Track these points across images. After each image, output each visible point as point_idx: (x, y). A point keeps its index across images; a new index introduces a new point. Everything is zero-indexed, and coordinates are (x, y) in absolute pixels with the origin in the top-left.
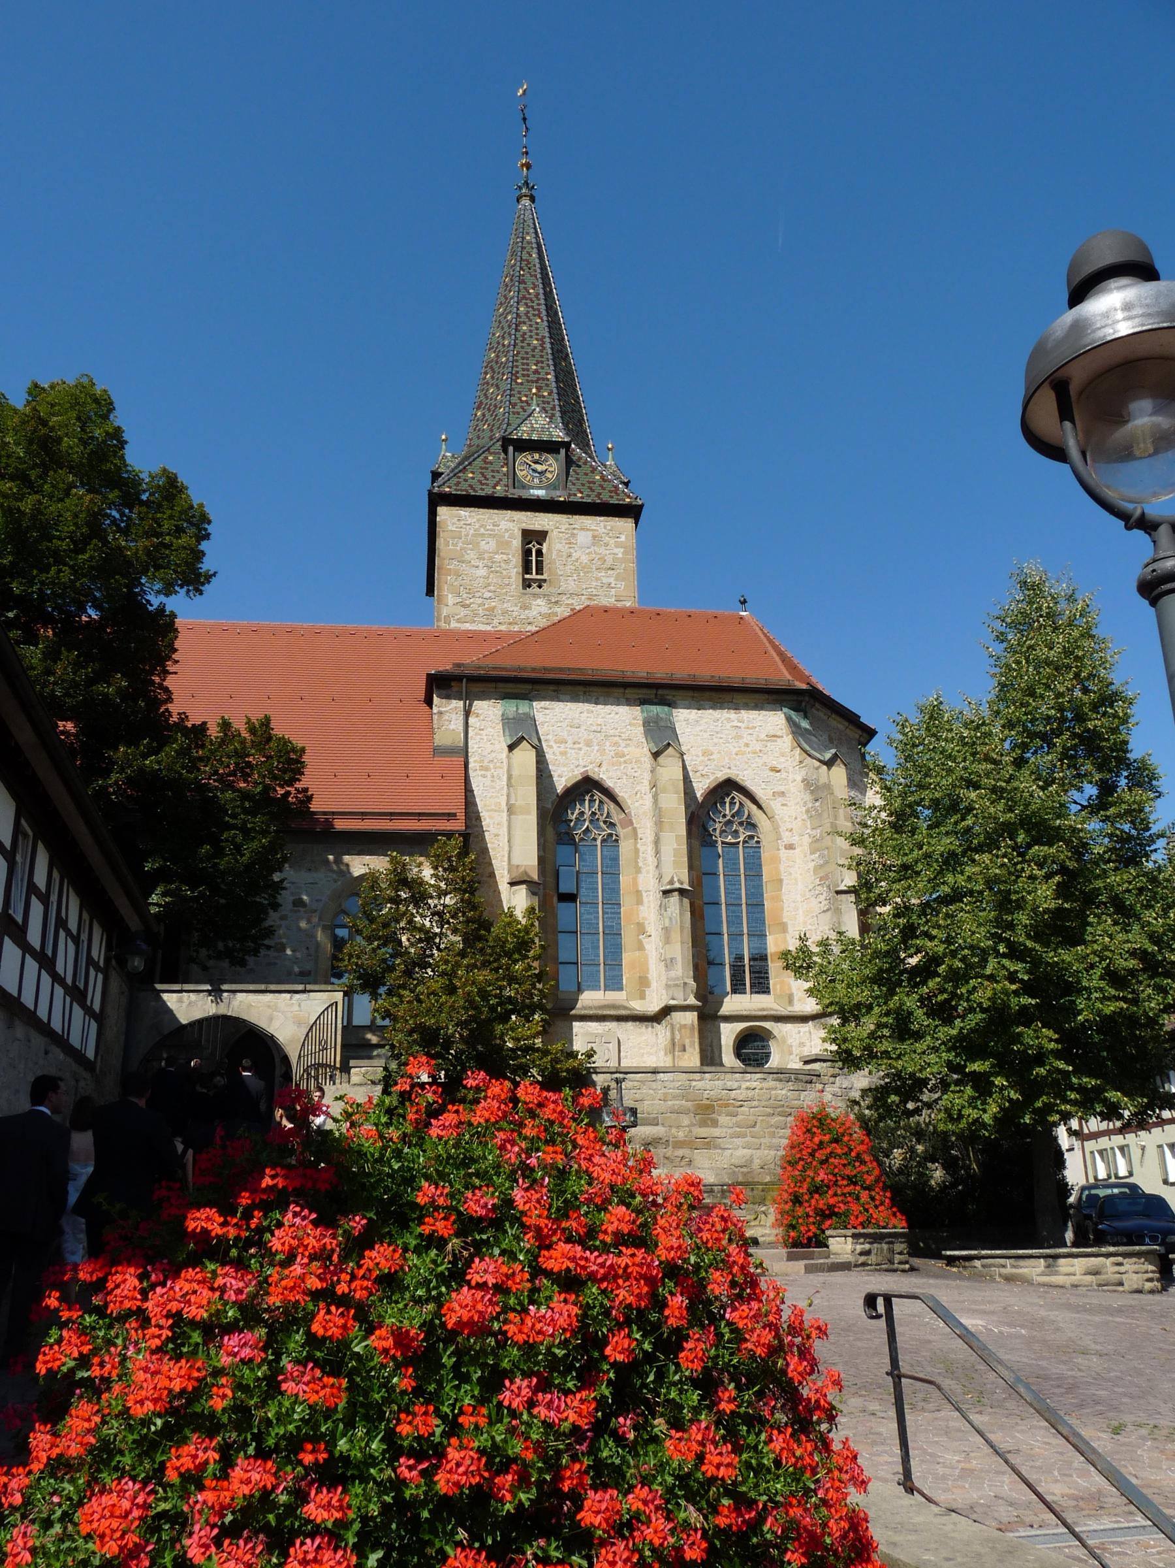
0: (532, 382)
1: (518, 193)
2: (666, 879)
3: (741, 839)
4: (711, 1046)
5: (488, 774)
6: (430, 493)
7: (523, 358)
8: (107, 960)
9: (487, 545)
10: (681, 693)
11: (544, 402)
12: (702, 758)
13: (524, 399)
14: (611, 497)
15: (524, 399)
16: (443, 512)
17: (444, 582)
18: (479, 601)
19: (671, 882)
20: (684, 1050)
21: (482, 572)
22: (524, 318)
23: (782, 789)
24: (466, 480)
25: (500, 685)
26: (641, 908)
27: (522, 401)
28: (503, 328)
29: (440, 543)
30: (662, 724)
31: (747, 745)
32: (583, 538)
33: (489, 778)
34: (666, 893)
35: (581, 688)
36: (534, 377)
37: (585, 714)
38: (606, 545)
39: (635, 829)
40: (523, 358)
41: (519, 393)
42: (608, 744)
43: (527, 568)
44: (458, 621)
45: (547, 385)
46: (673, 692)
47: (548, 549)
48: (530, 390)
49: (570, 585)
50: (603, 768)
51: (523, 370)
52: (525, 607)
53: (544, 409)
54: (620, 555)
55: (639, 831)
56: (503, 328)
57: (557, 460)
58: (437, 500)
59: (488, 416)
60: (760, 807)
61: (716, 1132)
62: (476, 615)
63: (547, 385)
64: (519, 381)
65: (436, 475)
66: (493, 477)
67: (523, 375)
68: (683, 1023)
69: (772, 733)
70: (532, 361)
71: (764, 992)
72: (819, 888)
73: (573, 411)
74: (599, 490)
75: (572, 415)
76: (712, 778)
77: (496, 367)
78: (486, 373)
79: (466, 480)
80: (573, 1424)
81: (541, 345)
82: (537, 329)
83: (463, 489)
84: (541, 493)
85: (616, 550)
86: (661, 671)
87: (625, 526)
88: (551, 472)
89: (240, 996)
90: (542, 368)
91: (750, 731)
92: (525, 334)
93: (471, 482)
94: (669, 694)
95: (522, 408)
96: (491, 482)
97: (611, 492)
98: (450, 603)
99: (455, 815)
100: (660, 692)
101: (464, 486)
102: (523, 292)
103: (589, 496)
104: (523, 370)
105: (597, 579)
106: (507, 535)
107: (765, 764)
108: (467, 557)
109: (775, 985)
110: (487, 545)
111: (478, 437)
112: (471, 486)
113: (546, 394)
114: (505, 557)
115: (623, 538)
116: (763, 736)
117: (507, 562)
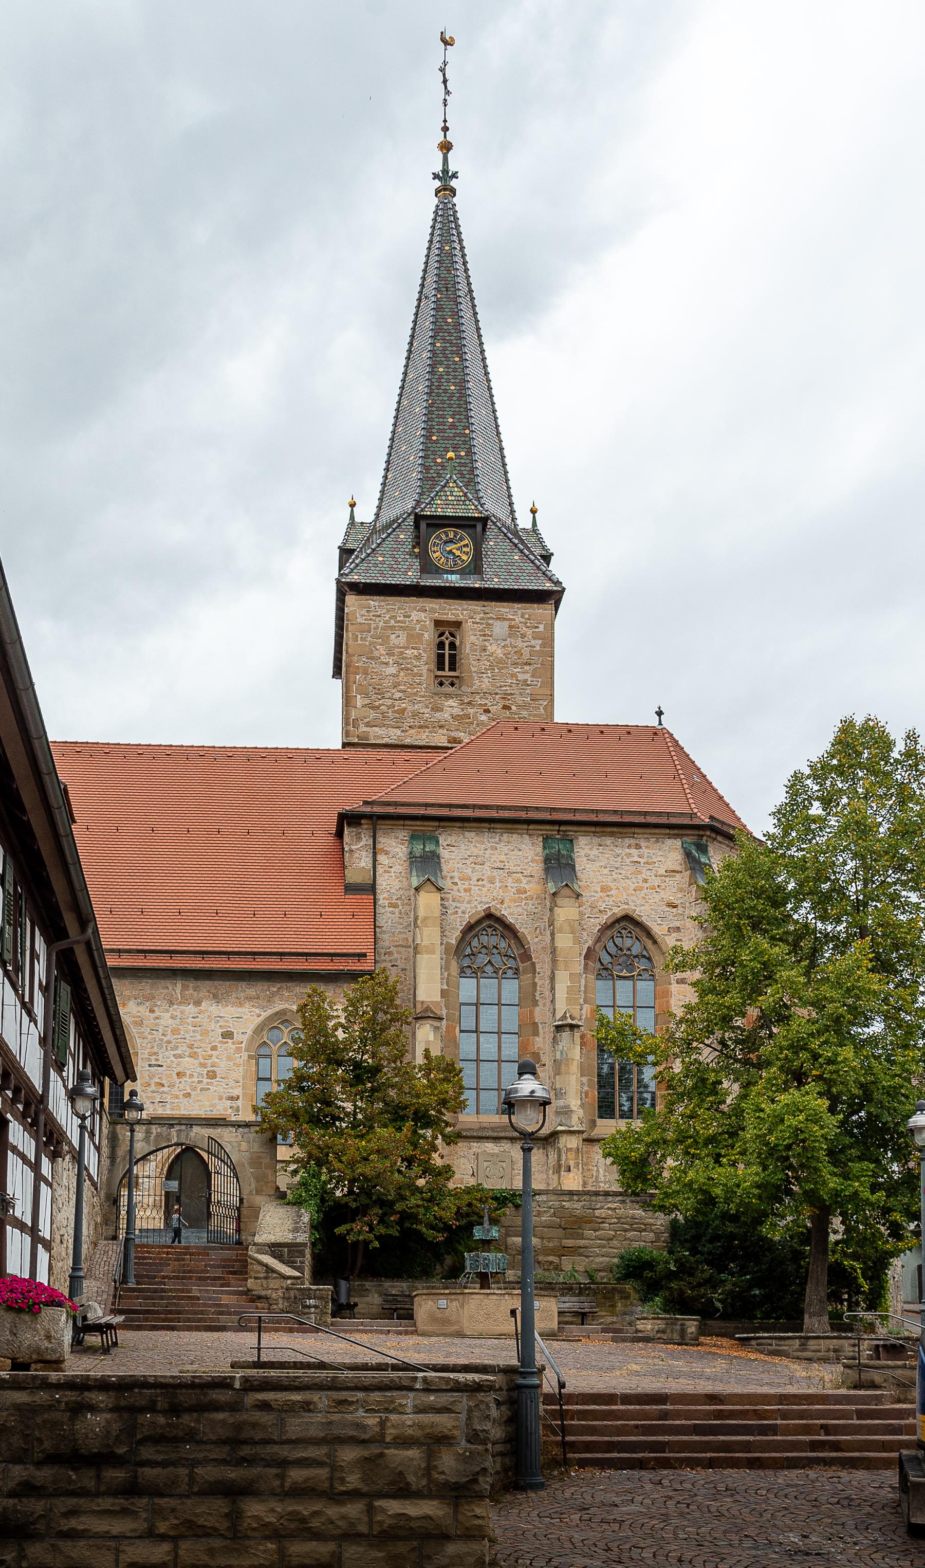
0: (448, 439)
2: (559, 1015)
6: (338, 582)
7: (438, 409)
9: (398, 639)
13: (439, 460)
15: (439, 460)
18: (389, 702)
19: (564, 1017)
20: (569, 1171)
21: (392, 670)
23: (678, 924)
26: (537, 1039)
31: (645, 881)
32: (500, 629)
33: (397, 915)
34: (559, 1028)
36: (450, 433)
37: (489, 851)
42: (510, 880)
43: (440, 666)
44: (368, 725)
47: (461, 642)
50: (505, 905)
52: (437, 709)
54: (538, 648)
55: (537, 966)
60: (655, 942)
61: (582, 1242)
64: (434, 438)
69: (671, 868)
76: (609, 914)
84: (454, 580)
85: (533, 642)
90: (460, 421)
91: (650, 867)
98: (359, 704)
99: (365, 955)
100: (562, 828)
105: (513, 675)
108: (376, 654)
110: (398, 639)
113: (463, 454)
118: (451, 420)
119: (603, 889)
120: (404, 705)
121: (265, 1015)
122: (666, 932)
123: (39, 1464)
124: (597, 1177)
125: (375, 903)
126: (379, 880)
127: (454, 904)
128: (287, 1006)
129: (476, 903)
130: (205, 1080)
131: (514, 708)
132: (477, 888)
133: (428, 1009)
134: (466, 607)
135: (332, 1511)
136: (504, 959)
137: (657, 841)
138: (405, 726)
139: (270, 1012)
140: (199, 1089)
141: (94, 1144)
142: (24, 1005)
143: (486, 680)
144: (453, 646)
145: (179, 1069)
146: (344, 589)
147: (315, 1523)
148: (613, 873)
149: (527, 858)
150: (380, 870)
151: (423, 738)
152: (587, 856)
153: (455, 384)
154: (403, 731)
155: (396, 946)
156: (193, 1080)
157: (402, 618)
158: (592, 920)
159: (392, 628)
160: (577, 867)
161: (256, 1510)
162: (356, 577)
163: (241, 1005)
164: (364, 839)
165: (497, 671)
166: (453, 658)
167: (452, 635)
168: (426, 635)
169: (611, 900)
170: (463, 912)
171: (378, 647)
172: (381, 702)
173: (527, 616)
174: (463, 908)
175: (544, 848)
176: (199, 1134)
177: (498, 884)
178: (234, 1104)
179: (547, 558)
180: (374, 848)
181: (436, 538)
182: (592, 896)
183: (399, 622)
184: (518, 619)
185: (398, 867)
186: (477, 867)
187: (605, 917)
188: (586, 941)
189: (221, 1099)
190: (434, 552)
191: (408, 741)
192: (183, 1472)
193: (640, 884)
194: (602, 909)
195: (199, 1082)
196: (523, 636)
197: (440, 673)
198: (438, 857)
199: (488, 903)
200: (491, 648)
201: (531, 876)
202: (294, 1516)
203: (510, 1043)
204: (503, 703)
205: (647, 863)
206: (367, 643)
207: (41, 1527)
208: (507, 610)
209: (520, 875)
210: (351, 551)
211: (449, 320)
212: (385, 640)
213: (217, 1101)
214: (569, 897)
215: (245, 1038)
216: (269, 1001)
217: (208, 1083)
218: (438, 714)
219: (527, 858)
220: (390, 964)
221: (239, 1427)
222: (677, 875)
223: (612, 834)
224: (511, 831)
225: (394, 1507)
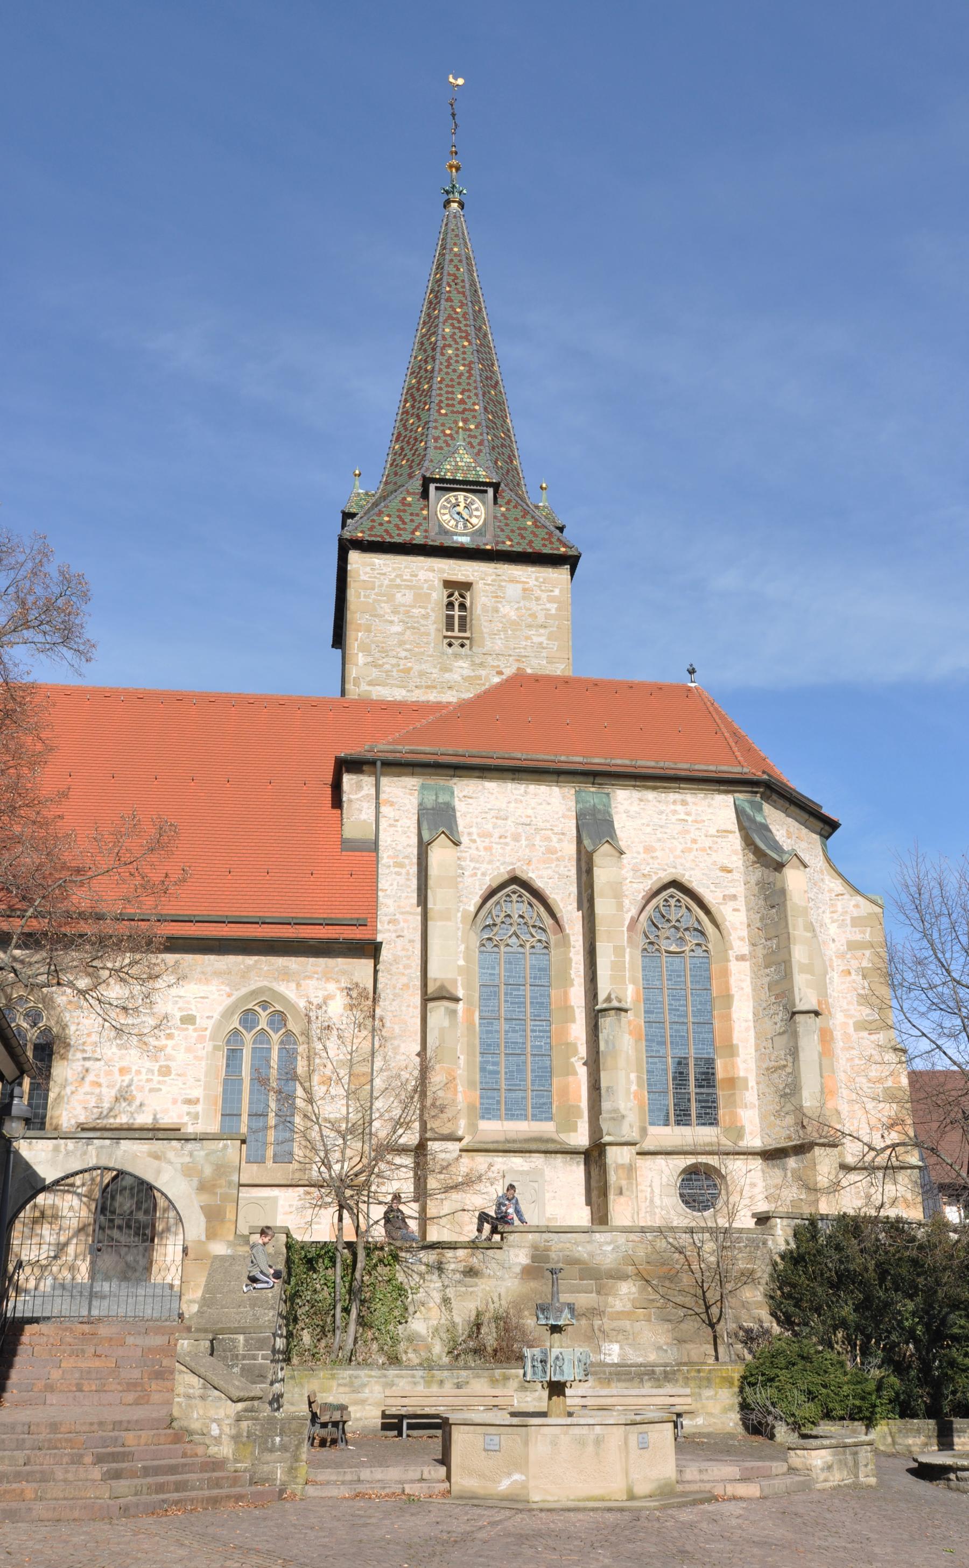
0: (458, 412)
1: (445, 197)
3: (687, 948)
4: (650, 1186)
5: (404, 871)
6: (341, 540)
7: (447, 386)
9: (404, 598)
11: (470, 436)
12: (643, 856)
13: (448, 432)
14: (544, 545)
15: (448, 432)
16: (354, 557)
17: (355, 638)
18: (394, 661)
19: (608, 999)
20: (621, 1193)
21: (397, 628)
22: (450, 341)
24: (381, 524)
27: (446, 435)
28: (425, 351)
30: (600, 817)
31: (694, 841)
32: (513, 591)
36: (459, 408)
37: (513, 805)
38: (538, 599)
40: (447, 386)
41: (443, 425)
42: (538, 838)
43: (450, 626)
44: (370, 683)
45: (474, 417)
47: (472, 603)
48: (456, 422)
49: (498, 644)
51: (447, 399)
52: (445, 669)
53: (470, 443)
54: (553, 611)
56: (425, 351)
57: (484, 503)
59: (407, 451)
60: (707, 912)
63: (474, 417)
64: (443, 411)
65: (347, 516)
66: (412, 521)
67: (448, 405)
68: (620, 1161)
69: (723, 827)
70: (458, 389)
71: (711, 1124)
72: (774, 1007)
73: (503, 446)
74: (531, 537)
75: (502, 448)
76: (655, 878)
77: (417, 395)
78: (406, 401)
79: (381, 524)
80: (575, 1130)
81: (469, 372)
82: (464, 353)
83: (377, 535)
84: (465, 540)
85: (548, 606)
86: (598, 761)
87: (560, 575)
90: (469, 397)
91: (699, 826)
92: (450, 358)
93: (387, 526)
95: (446, 442)
97: (543, 539)
101: (379, 531)
102: (450, 311)
103: (518, 543)
104: (447, 399)
105: (528, 638)
106: (426, 586)
107: (715, 863)
108: (381, 612)
109: (724, 1115)
110: (404, 598)
111: (396, 474)
112: (386, 531)
113: (472, 427)
114: (423, 611)
115: (557, 592)
117: (425, 617)
118: (460, 396)
120: (409, 665)
121: (237, 995)
122: (721, 901)
124: (652, 1201)
127: (472, 865)
128: (266, 983)
129: (498, 864)
130: (156, 1078)
132: (499, 846)
133: (442, 987)
134: (477, 568)
136: (533, 930)
138: (411, 685)
139: (244, 991)
140: (147, 1089)
143: (499, 642)
144: (462, 606)
145: (124, 1064)
146: (345, 547)
148: (658, 832)
149: (557, 813)
150: (383, 824)
152: (626, 812)
153: (464, 365)
154: (408, 691)
155: (402, 913)
156: (140, 1077)
157: (408, 577)
158: (635, 885)
159: (398, 586)
162: (360, 535)
163: (207, 982)
164: (366, 788)
165: (510, 632)
166: (463, 619)
167: (462, 596)
169: (656, 862)
170: (484, 874)
171: (383, 605)
172: (384, 660)
173: (541, 580)
174: (483, 870)
175: (577, 802)
176: (134, 1157)
177: (524, 842)
178: (193, 1109)
180: (377, 797)
181: (446, 500)
182: (633, 858)
183: (405, 580)
184: (532, 582)
185: (405, 820)
186: (500, 822)
187: (650, 882)
188: (629, 910)
189: (175, 1102)
190: (444, 514)
193: (689, 845)
194: (646, 872)
195: (148, 1080)
197: (449, 634)
198: (454, 809)
199: (512, 864)
201: (563, 834)
203: (540, 1031)
205: (696, 821)
206: (371, 601)
208: (520, 573)
209: (550, 832)
211: (458, 310)
212: (391, 598)
214: (611, 856)
215: (210, 1024)
216: (243, 977)
217: (159, 1082)
218: (447, 675)
219: (557, 813)
220: (394, 935)
222: (731, 835)
224: (538, 781)
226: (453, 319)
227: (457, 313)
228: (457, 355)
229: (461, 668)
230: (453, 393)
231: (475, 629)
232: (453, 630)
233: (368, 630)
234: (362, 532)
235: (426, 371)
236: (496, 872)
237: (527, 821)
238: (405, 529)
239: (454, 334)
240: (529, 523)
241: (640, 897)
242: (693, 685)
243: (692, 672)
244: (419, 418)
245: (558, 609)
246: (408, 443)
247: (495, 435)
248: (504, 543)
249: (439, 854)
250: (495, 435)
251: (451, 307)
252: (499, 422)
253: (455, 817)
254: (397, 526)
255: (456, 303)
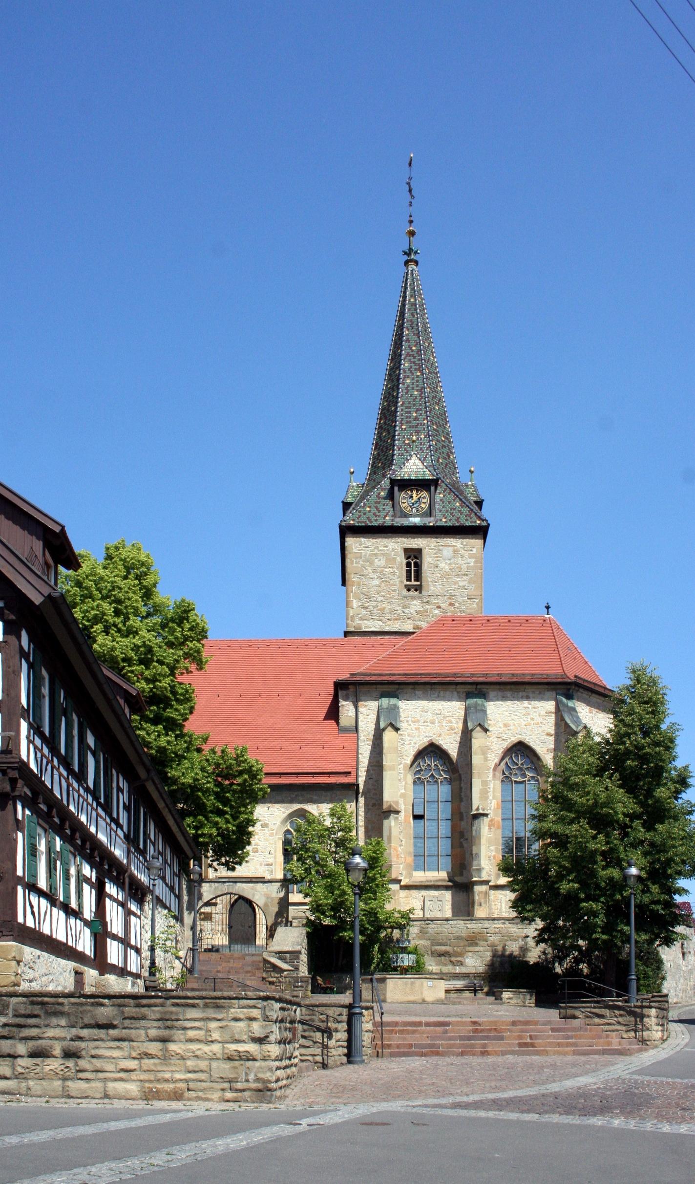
0: (413, 427)
1: (406, 258)
6: (341, 527)
8: (179, 871)
10: (492, 687)
14: (467, 520)
15: (407, 442)
16: (350, 541)
18: (374, 604)
19: (478, 809)
21: (377, 582)
25: (379, 686)
29: (348, 561)
30: (479, 708)
31: (532, 719)
35: (428, 686)
36: (414, 423)
39: (460, 775)
44: (361, 619)
46: (487, 687)
51: (407, 417)
54: (472, 564)
58: (346, 531)
62: (372, 614)
65: (346, 506)
67: (407, 422)
73: (443, 446)
74: (457, 515)
76: (509, 741)
79: (365, 514)
84: (416, 521)
85: (469, 560)
87: (475, 543)
88: (424, 498)
89: (238, 884)
94: (484, 688)
96: (382, 514)
98: (355, 606)
99: (350, 773)
100: (479, 687)
101: (364, 518)
105: (455, 583)
108: (365, 572)
110: (380, 562)
112: (368, 518)
113: (422, 436)
115: (474, 551)
116: (543, 713)
117: (394, 573)
118: (414, 415)
119: (505, 725)
123: (82, 1028)
125: (358, 739)
126: (360, 724)
131: (457, 604)
135: (206, 1048)
137: (540, 693)
141: (175, 894)
142: (112, 820)
146: (346, 531)
147: (198, 1053)
150: (361, 717)
151: (396, 627)
153: (417, 391)
159: (376, 555)
160: (488, 712)
161: (172, 1047)
162: (352, 522)
168: (398, 558)
178: (269, 868)
179: (479, 504)
189: (261, 865)
191: (387, 629)
192: (142, 1032)
196: (462, 557)
197: (408, 583)
200: (442, 565)
202: (188, 1050)
204: (449, 601)
207: (83, 1053)
210: (351, 504)
212: (371, 564)
213: (258, 867)
221: (165, 1013)
223: (511, 690)
225: (233, 1047)
226: (410, 355)
227: (413, 351)
228: (413, 384)
229: (416, 605)
230: (410, 412)
231: (423, 579)
232: (410, 581)
233: (359, 584)
234: (353, 520)
235: (393, 396)
236: (421, 742)
237: (439, 712)
238: (379, 516)
239: (411, 367)
240: (458, 504)
241: (500, 752)
242: (547, 616)
243: (548, 608)
244: (389, 433)
245: (475, 562)
246: (382, 451)
247: (438, 441)
248: (441, 520)
249: (389, 736)
250: (438, 441)
251: (409, 346)
252: (440, 430)
253: (399, 712)
254: (374, 514)
255: (413, 343)
